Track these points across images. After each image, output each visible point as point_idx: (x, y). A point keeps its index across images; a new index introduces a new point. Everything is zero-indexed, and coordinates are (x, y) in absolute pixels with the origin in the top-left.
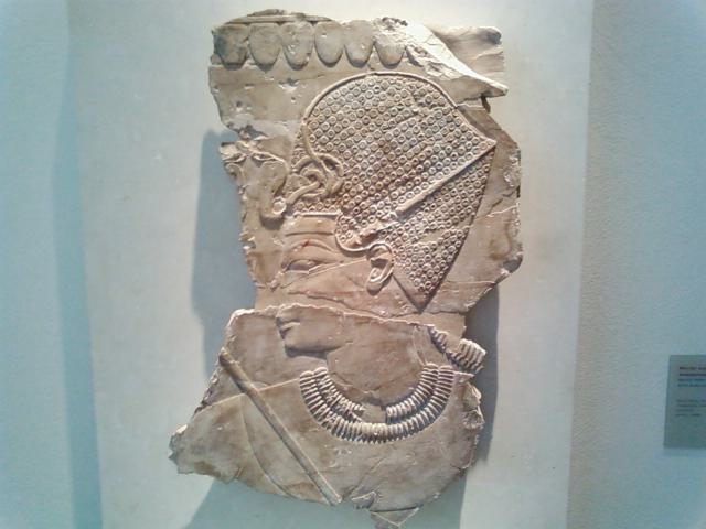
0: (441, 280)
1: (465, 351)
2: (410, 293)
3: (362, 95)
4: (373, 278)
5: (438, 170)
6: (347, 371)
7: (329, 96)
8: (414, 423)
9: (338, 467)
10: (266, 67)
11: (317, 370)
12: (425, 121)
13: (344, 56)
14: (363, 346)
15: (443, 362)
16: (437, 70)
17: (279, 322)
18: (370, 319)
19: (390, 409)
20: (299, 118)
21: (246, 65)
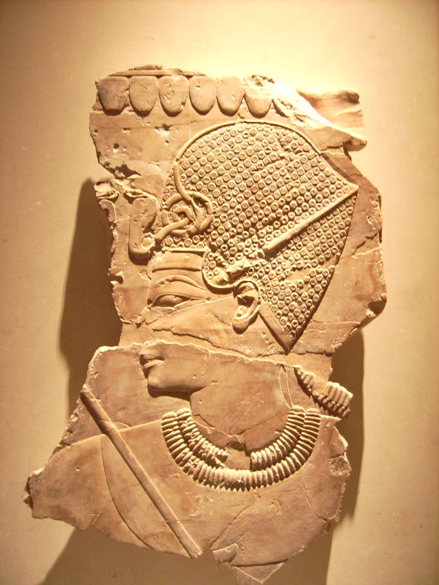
0: (308, 320)
1: (332, 393)
2: (277, 332)
3: (232, 139)
4: (239, 315)
5: (304, 211)
6: (211, 413)
7: (201, 140)
8: (279, 470)
9: (200, 516)
10: (143, 114)
11: (180, 411)
12: (291, 164)
13: (216, 106)
14: (229, 387)
15: (310, 405)
16: (301, 121)
17: (143, 360)
18: (236, 358)
19: (253, 454)
20: (172, 160)
21: (126, 111)
